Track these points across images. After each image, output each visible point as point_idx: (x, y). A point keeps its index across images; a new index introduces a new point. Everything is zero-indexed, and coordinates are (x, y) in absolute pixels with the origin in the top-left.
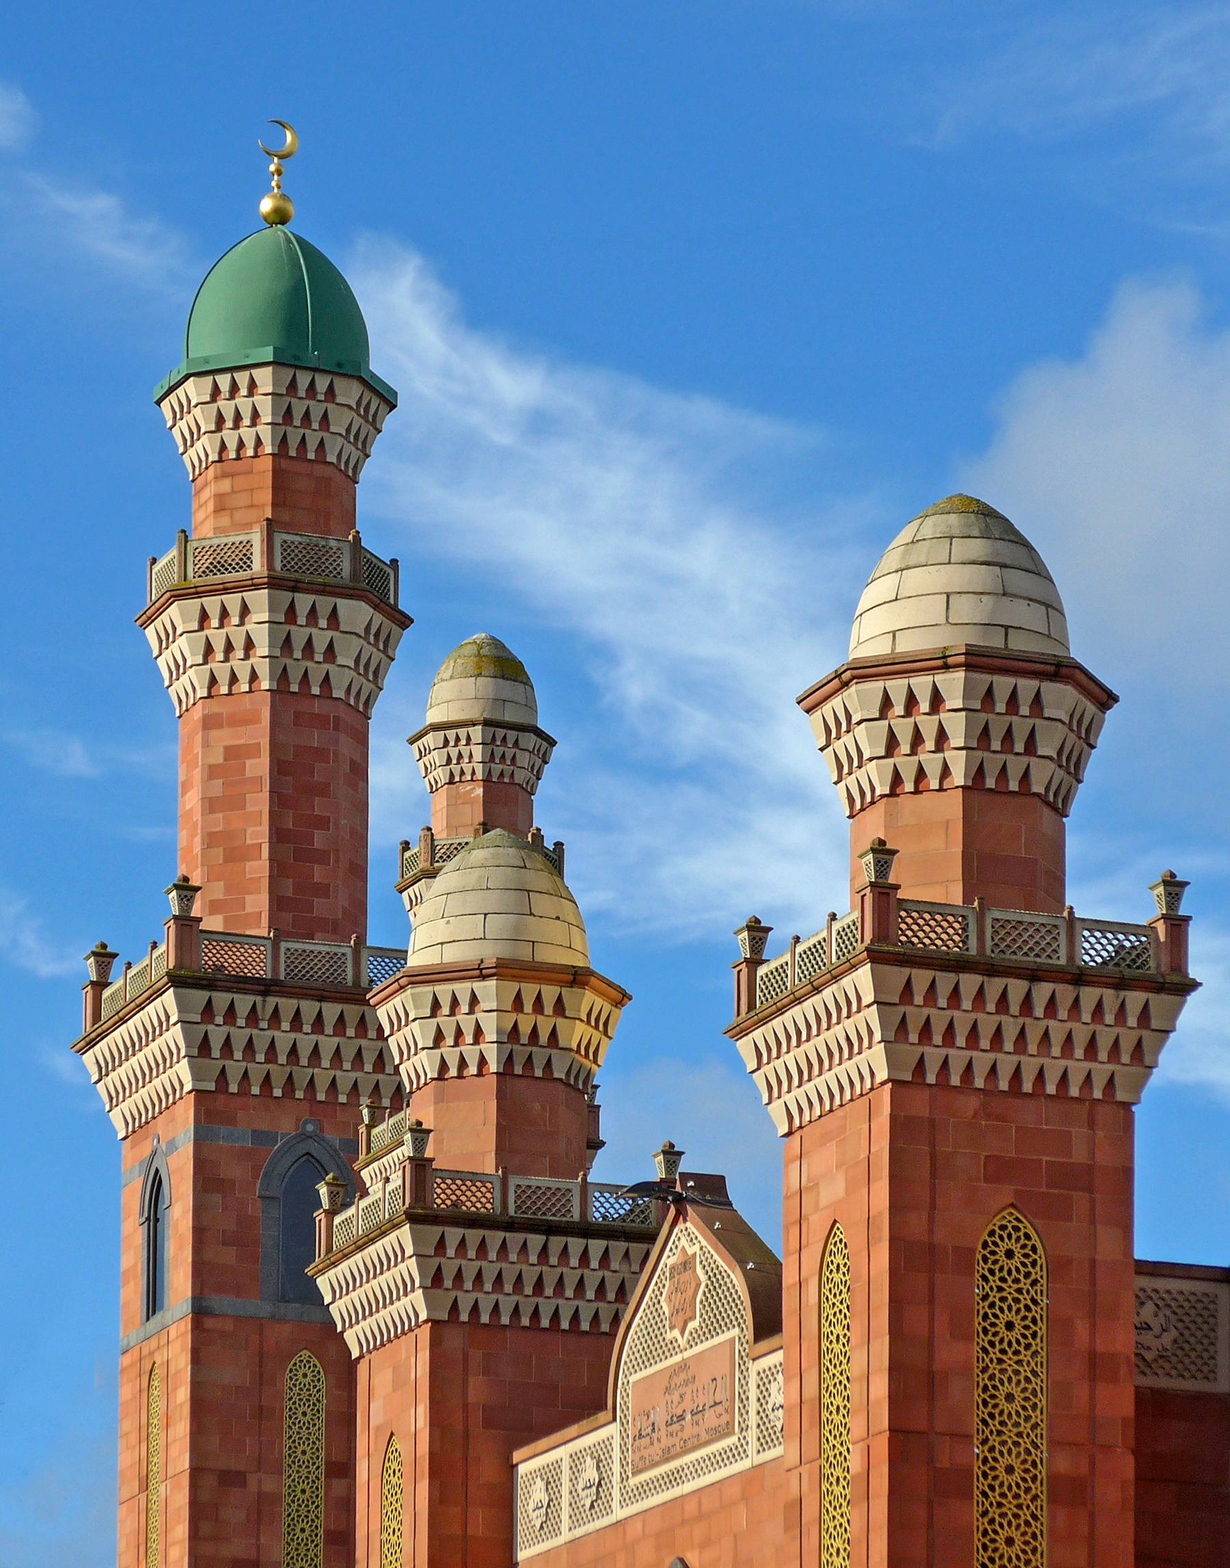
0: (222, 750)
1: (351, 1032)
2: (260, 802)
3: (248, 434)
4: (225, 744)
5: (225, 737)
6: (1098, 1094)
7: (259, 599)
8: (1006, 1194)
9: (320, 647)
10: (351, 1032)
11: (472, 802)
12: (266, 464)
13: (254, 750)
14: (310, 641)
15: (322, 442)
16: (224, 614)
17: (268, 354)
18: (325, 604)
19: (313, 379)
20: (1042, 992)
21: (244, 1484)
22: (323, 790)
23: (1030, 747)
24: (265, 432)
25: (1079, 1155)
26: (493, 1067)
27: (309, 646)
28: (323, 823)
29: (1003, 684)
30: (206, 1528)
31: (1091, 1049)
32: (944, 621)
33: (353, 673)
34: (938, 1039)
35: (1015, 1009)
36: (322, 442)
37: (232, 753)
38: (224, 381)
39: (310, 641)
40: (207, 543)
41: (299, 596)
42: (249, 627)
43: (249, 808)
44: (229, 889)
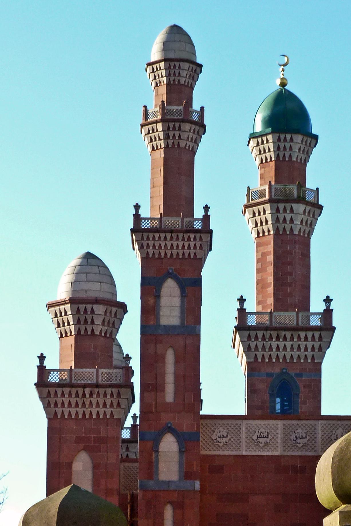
0: (261, 253)
1: (295, 340)
2: (271, 269)
3: (268, 155)
4: (262, 251)
6: (108, 417)
7: (267, 206)
8: (81, 446)
9: (288, 219)
10: (295, 340)
12: (273, 163)
14: (285, 218)
15: (290, 155)
17: (269, 130)
18: (288, 206)
19: (279, 136)
20: (87, 391)
22: (290, 264)
23: (93, 322)
24: (272, 154)
25: (103, 434)
27: (285, 220)
28: (291, 274)
29: (82, 307)
31: (105, 405)
33: (301, 226)
34: (59, 406)
35: (80, 396)
36: (290, 155)
38: (260, 140)
39: (285, 218)
40: (259, 189)
41: (279, 204)
43: (268, 271)
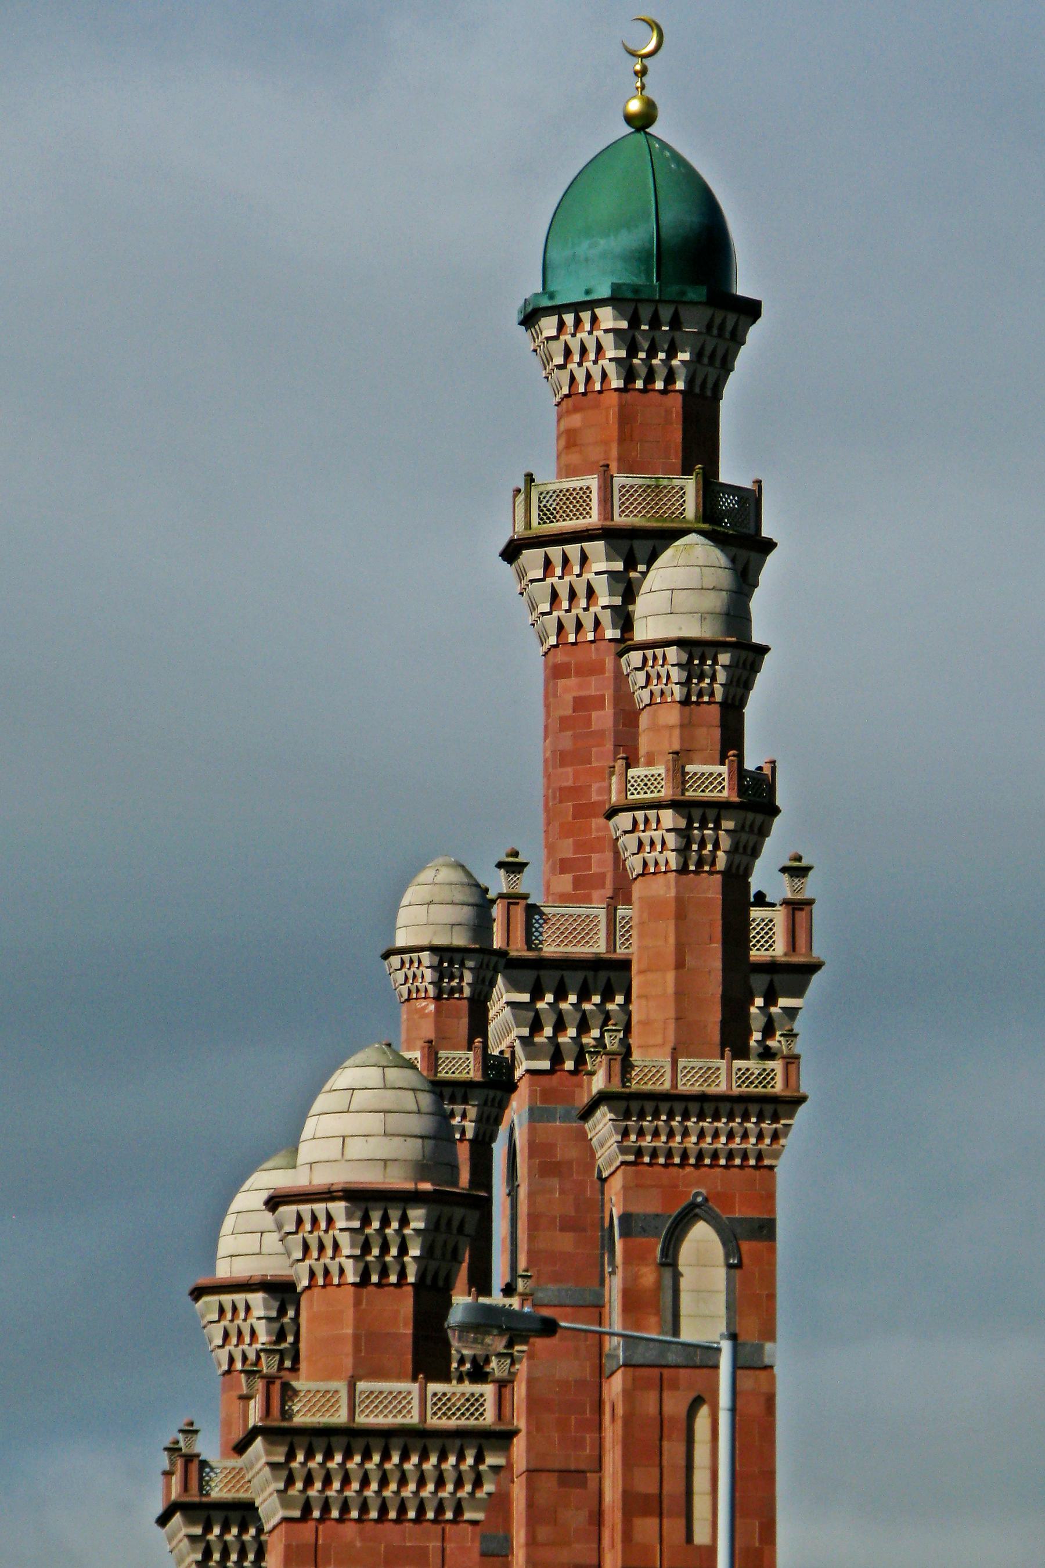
5: (570, 687)
11: (426, 1016)
13: (598, 702)
16: (566, 561)
21: (584, 1484)
26: (411, 1279)
30: (543, 1533)
32: (339, 1157)
37: (582, 704)
42: (589, 576)
44: (578, 847)
